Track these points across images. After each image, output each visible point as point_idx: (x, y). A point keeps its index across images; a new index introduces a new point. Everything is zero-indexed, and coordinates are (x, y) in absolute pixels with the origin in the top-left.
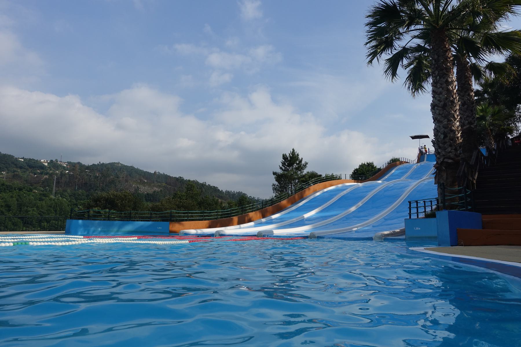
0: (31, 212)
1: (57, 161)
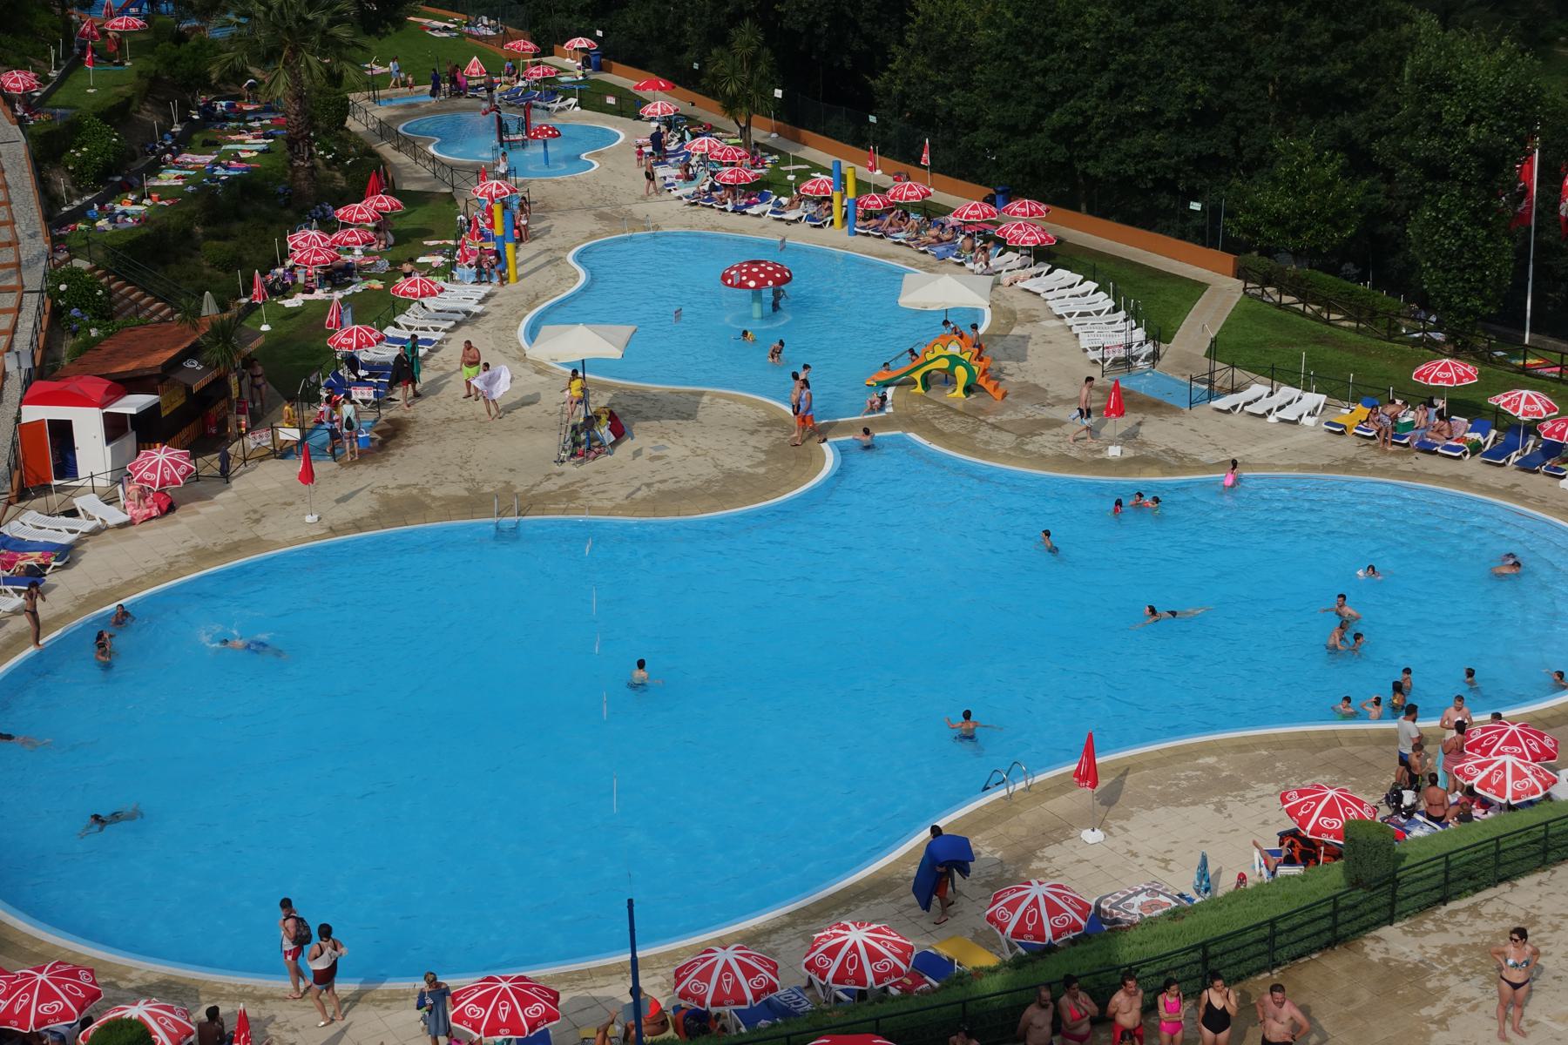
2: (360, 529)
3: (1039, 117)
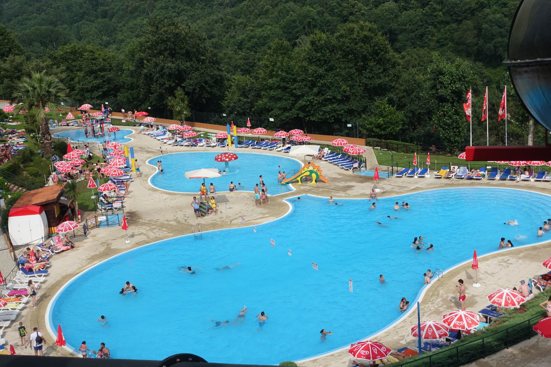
2: (140, 245)
3: (293, 105)
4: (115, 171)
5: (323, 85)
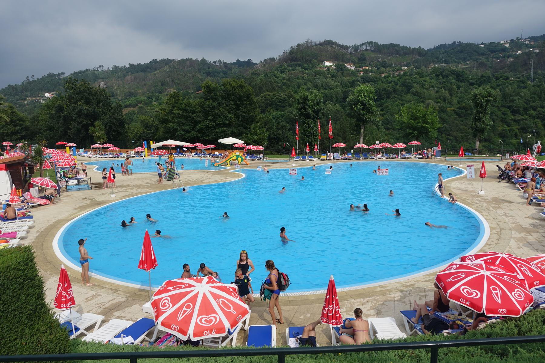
0: (517, 101)
1: (517, 39)
4: (68, 157)
5: (215, 114)
